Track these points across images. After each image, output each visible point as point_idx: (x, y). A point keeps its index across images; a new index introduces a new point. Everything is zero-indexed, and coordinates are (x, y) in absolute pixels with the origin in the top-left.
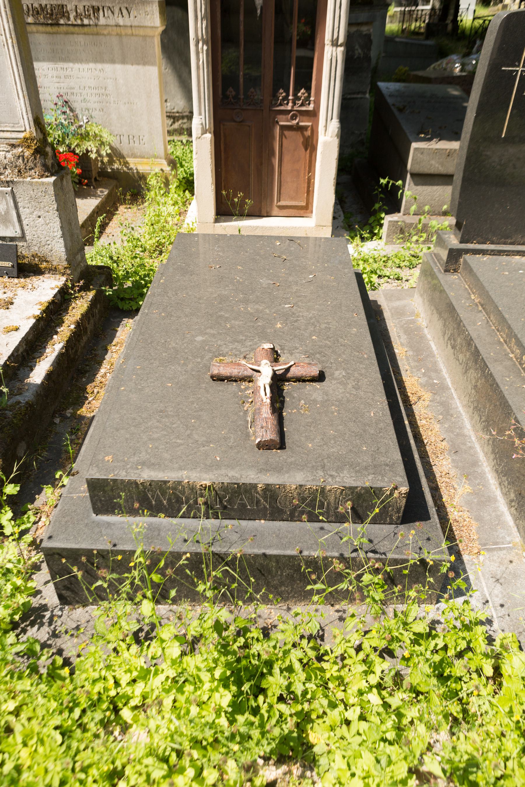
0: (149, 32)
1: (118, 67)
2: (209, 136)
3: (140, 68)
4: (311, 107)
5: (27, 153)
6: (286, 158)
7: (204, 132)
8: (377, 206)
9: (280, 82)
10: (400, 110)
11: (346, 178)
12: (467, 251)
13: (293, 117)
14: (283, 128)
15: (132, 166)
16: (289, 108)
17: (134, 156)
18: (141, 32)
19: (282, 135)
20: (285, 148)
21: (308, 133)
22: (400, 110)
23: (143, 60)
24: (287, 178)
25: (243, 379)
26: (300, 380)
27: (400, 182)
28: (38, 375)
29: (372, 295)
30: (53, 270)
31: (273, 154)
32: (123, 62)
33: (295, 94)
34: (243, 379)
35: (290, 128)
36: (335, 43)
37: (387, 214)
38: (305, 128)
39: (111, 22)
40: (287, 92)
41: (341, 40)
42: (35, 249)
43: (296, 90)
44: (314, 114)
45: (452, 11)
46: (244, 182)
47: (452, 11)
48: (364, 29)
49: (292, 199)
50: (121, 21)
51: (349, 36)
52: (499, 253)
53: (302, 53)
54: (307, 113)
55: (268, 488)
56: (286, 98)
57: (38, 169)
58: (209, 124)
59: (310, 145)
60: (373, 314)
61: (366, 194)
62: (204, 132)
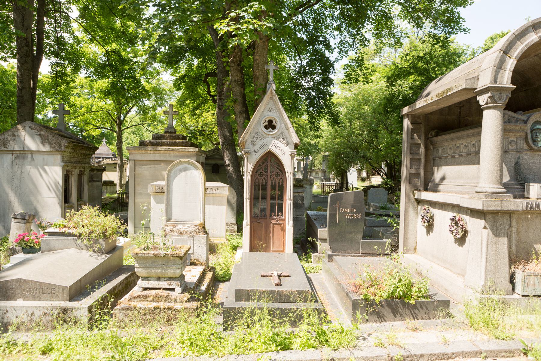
0: (224, 195)
1: (211, 206)
2: (249, 227)
3: (220, 207)
4: (283, 218)
5: (200, 228)
6: (275, 234)
7: (247, 225)
8: (309, 250)
9: (272, 210)
10: (315, 220)
11: (298, 246)
12: (334, 255)
13: (277, 221)
14: (274, 224)
15: (212, 241)
16: (276, 218)
17: (213, 237)
18: (221, 195)
19: (273, 227)
20: (275, 231)
21: (282, 226)
22: (315, 220)
23: (221, 204)
24: (276, 241)
25: (269, 276)
26: (285, 276)
27: (315, 239)
28: (203, 288)
29: (308, 275)
30: (201, 264)
31: (270, 232)
32: (214, 204)
33: (278, 214)
34: (269, 276)
35: (276, 224)
36: (290, 200)
37: (313, 253)
38: (281, 224)
39: (211, 192)
40: (275, 213)
41: (292, 198)
42: (196, 257)
43: (278, 213)
44: (284, 220)
45: (345, 184)
46: (260, 241)
47: (345, 184)
48: (301, 194)
49: (278, 248)
50: (215, 192)
51: (294, 197)
52: (344, 256)
53: (280, 202)
54: (282, 220)
55: (278, 291)
56: (275, 215)
57: (202, 232)
58: (249, 223)
59: (283, 229)
60: (309, 279)
61: (305, 245)
62: (247, 225)
